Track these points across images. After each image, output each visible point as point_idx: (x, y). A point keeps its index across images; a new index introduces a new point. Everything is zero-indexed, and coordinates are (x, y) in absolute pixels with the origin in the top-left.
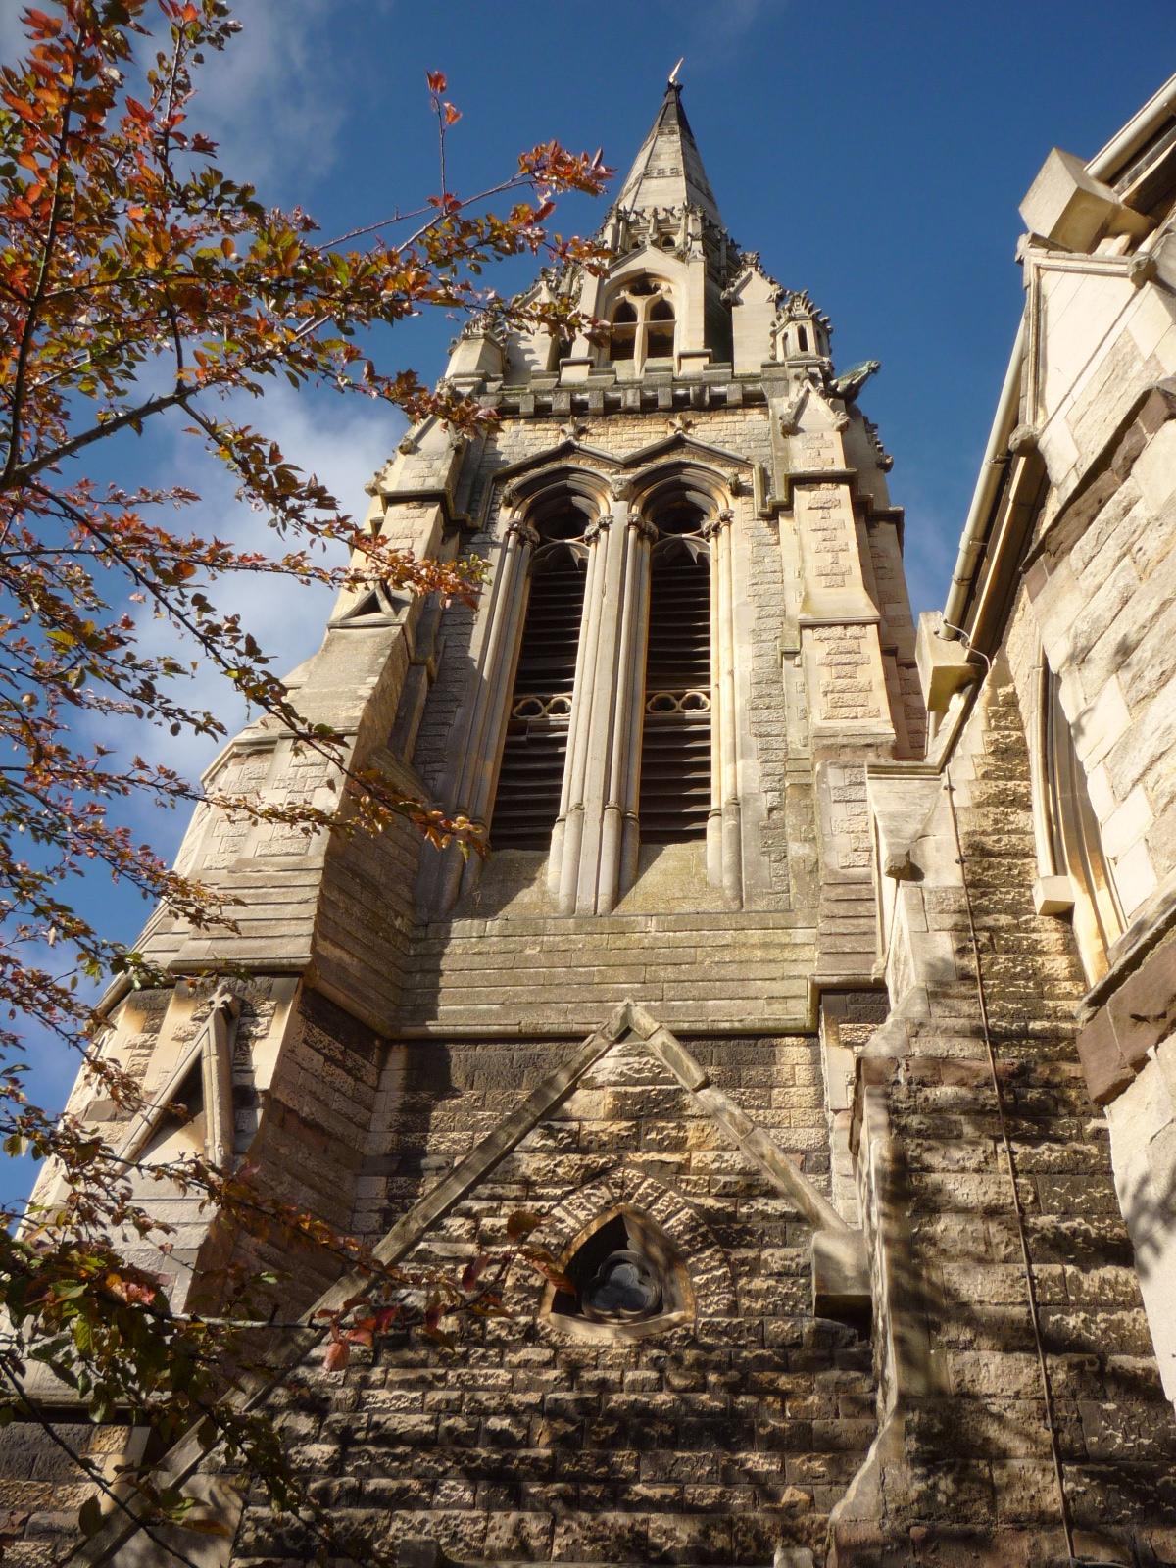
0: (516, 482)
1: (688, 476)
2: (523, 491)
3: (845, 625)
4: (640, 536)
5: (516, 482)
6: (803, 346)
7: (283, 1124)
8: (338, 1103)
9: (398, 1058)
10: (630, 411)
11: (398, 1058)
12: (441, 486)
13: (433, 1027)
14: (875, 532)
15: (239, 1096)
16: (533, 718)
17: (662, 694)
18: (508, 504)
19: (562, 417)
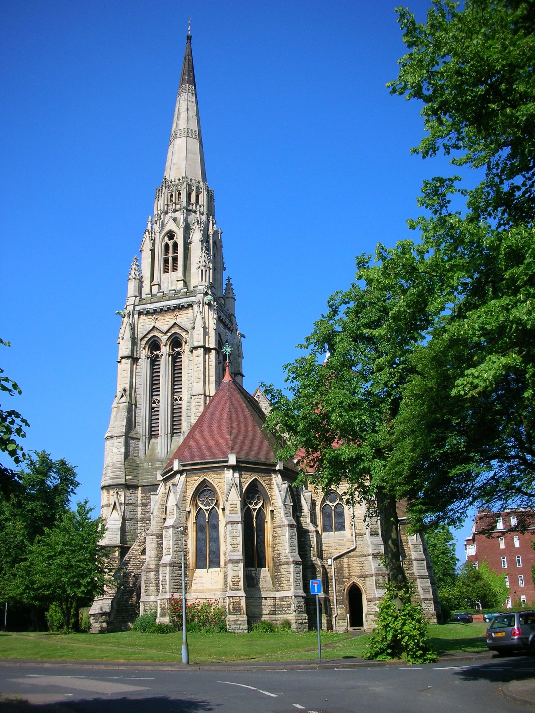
0: (146, 339)
3: (199, 395)
6: (202, 281)
9: (140, 488)
10: (166, 311)
18: (144, 348)
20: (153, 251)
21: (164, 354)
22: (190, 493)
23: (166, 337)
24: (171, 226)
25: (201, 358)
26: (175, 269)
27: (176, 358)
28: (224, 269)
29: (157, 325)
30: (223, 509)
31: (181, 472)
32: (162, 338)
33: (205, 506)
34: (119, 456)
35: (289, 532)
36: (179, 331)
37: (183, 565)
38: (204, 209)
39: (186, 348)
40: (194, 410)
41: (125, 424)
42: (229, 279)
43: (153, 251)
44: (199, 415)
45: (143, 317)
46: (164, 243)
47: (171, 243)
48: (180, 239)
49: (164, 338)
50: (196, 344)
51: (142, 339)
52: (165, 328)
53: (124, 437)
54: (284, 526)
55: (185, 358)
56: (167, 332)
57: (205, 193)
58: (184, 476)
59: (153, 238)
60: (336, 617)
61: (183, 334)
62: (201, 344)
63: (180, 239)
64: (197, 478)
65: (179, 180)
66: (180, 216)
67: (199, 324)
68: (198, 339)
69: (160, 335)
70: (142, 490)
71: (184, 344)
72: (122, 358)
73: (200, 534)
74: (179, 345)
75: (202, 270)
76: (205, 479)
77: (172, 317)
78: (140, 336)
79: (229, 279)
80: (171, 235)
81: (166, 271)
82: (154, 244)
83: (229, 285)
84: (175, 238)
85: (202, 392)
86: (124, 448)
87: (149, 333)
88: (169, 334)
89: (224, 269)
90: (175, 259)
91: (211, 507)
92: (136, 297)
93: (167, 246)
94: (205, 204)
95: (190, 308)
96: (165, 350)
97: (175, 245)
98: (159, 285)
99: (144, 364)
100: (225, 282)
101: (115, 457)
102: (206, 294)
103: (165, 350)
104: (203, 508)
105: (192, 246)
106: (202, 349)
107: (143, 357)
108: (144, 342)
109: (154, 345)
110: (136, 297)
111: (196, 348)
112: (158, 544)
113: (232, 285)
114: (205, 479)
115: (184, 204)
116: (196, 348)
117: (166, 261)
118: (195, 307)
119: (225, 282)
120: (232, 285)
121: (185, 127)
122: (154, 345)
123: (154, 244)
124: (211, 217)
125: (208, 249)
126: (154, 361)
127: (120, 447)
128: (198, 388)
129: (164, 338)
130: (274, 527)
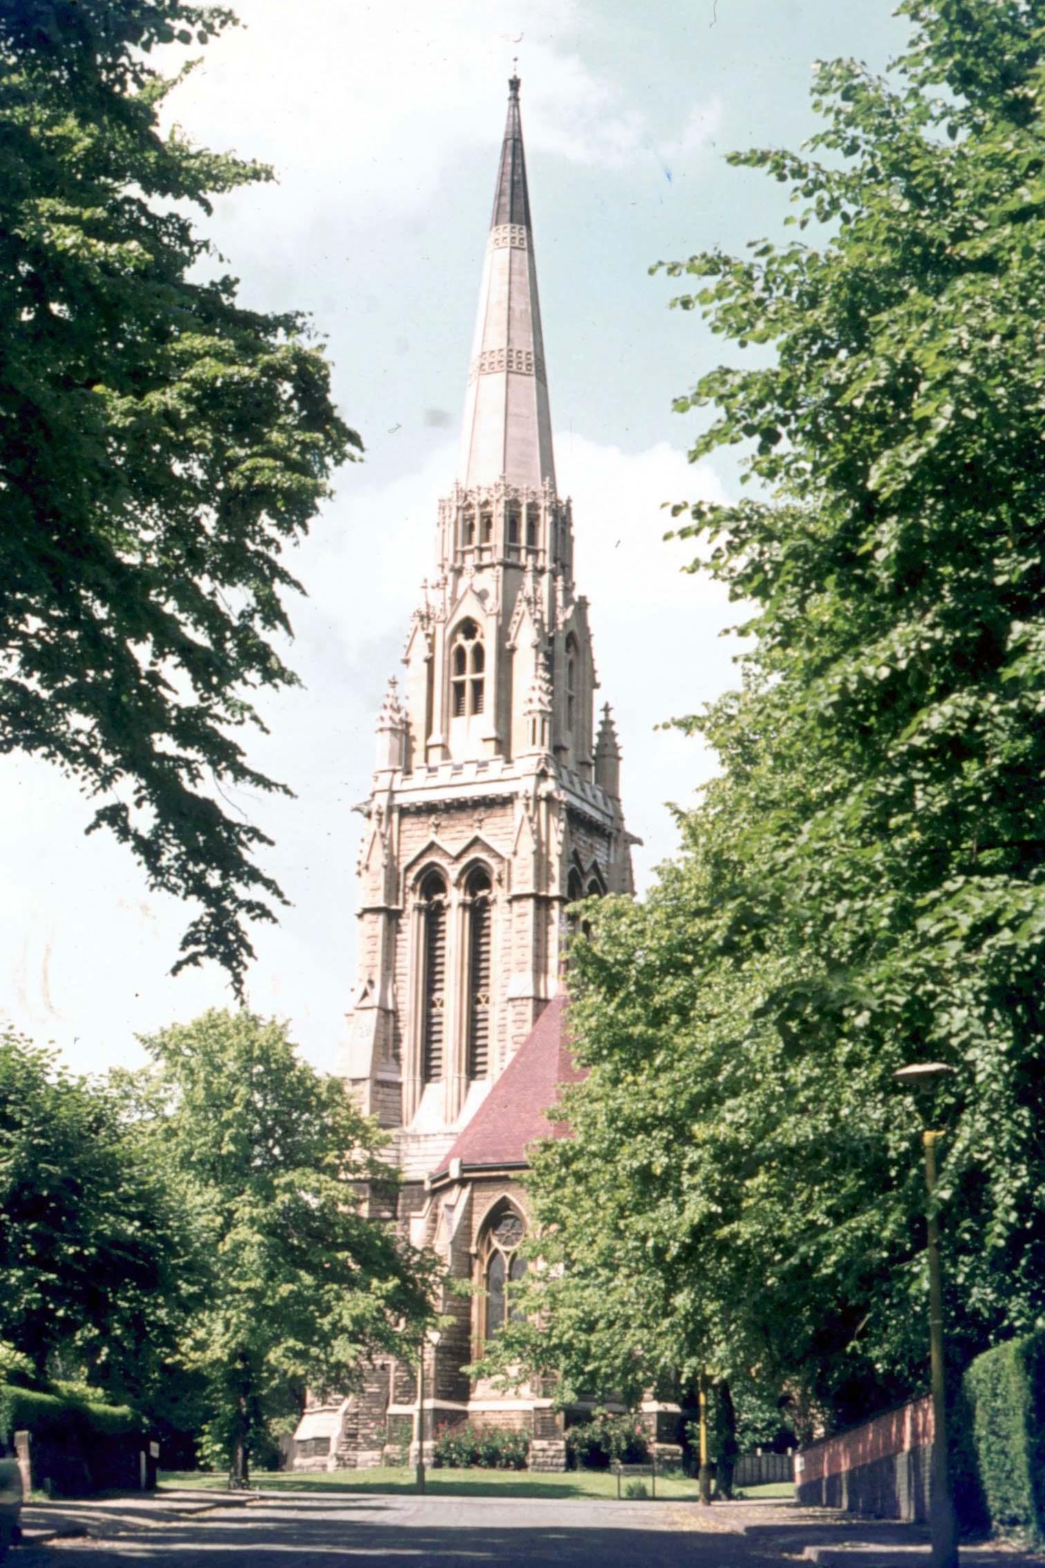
0: (417, 869)
2: (417, 878)
20: (430, 662)
21: (455, 905)
22: (478, 1221)
23: (459, 866)
24: (469, 608)
25: (529, 921)
26: (476, 709)
27: (478, 914)
28: (597, 686)
29: (438, 840)
31: (462, 1182)
32: (448, 868)
33: (505, 1243)
36: (483, 856)
37: (935, 1356)
38: (545, 561)
39: (498, 893)
40: (512, 1030)
42: (606, 709)
43: (430, 662)
44: (523, 1039)
45: (408, 823)
46: (455, 646)
47: (468, 645)
48: (488, 638)
49: (453, 872)
50: (516, 890)
51: (408, 868)
52: (454, 849)
55: (498, 916)
56: (458, 858)
57: (549, 519)
58: (468, 1189)
59: (390, 1006)
61: (492, 862)
62: (530, 889)
63: (488, 638)
66: (490, 581)
67: (528, 845)
68: (524, 881)
69: (443, 862)
70: (673, 1415)
71: (495, 884)
74: (486, 884)
76: (504, 1199)
77: (470, 821)
78: (405, 861)
79: (606, 709)
80: (469, 627)
81: (458, 712)
82: (432, 647)
83: (607, 723)
84: (478, 635)
85: (530, 992)
87: (422, 855)
88: (465, 860)
89: (597, 686)
90: (478, 686)
92: (394, 771)
93: (460, 652)
94: (547, 548)
96: (454, 896)
97: (479, 652)
98: (444, 746)
99: (412, 927)
100: (598, 716)
102: (542, 775)
103: (454, 896)
104: (502, 1248)
105: (517, 658)
107: (410, 907)
108: (412, 875)
109: (432, 882)
110: (394, 771)
113: (612, 723)
114: (504, 1199)
115: (499, 555)
116: (518, 898)
117: (459, 687)
118: (519, 805)
119: (597, 728)
120: (612, 723)
121: (504, 345)
122: (432, 882)
123: (432, 647)
124: (560, 578)
125: (549, 668)
126: (433, 916)
128: (523, 984)
129: (453, 872)
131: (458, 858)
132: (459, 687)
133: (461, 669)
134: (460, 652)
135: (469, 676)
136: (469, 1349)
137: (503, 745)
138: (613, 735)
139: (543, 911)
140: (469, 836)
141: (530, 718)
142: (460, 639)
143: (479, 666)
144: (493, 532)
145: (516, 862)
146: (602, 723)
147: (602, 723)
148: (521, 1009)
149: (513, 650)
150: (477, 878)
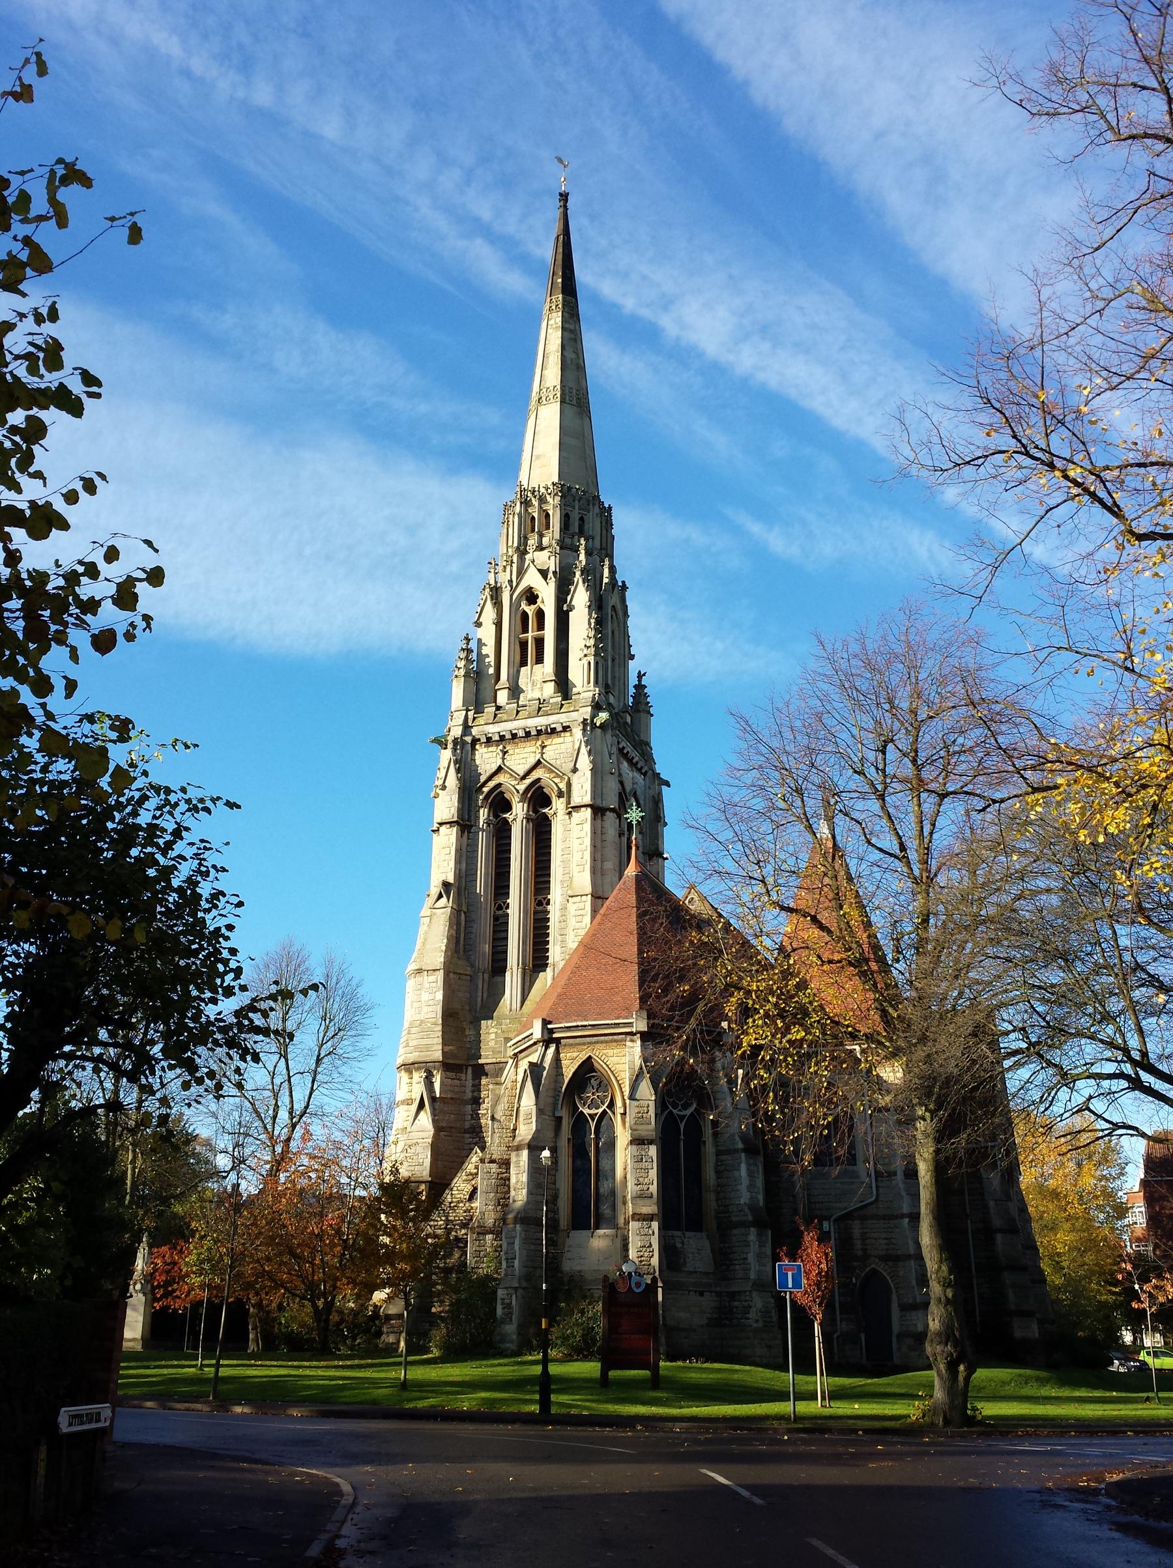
0: (486, 790)
1: (542, 783)
4: (528, 822)
5: (486, 790)
7: (444, 1103)
8: (457, 1089)
11: (470, 1070)
12: (455, 819)
13: (480, 1061)
14: (605, 818)
15: (433, 1099)
16: (501, 912)
17: (539, 898)
19: (498, 743)
23: (522, 787)
26: (539, 659)
28: (632, 657)
30: (624, 1114)
34: (431, 1009)
35: (748, 1165)
39: (558, 805)
41: (444, 948)
42: (640, 676)
53: (442, 971)
54: (736, 1151)
56: (524, 778)
60: (838, 1337)
64: (575, 1054)
65: (547, 488)
72: (441, 824)
73: (579, 1162)
75: (589, 663)
77: (533, 749)
80: (531, 596)
83: (640, 687)
84: (539, 601)
86: (442, 992)
89: (632, 657)
90: (539, 642)
91: (600, 1110)
95: (568, 734)
97: (540, 615)
100: (633, 680)
101: (425, 1009)
105: (572, 615)
106: (589, 810)
111: (577, 808)
112: (502, 1178)
116: (577, 808)
127: (435, 990)
130: (718, 1153)
131: (524, 778)
132: (524, 645)
133: (525, 630)
134: (525, 616)
135: (530, 635)
136: (919, 1214)
137: (563, 685)
138: (646, 696)
139: (599, 821)
140: (532, 761)
141: (585, 661)
142: (524, 606)
143: (541, 626)
144: (422, 940)
145: (575, 779)
146: (635, 687)
147: (635, 687)
148: (581, 906)
149: (571, 608)
150: (538, 798)
